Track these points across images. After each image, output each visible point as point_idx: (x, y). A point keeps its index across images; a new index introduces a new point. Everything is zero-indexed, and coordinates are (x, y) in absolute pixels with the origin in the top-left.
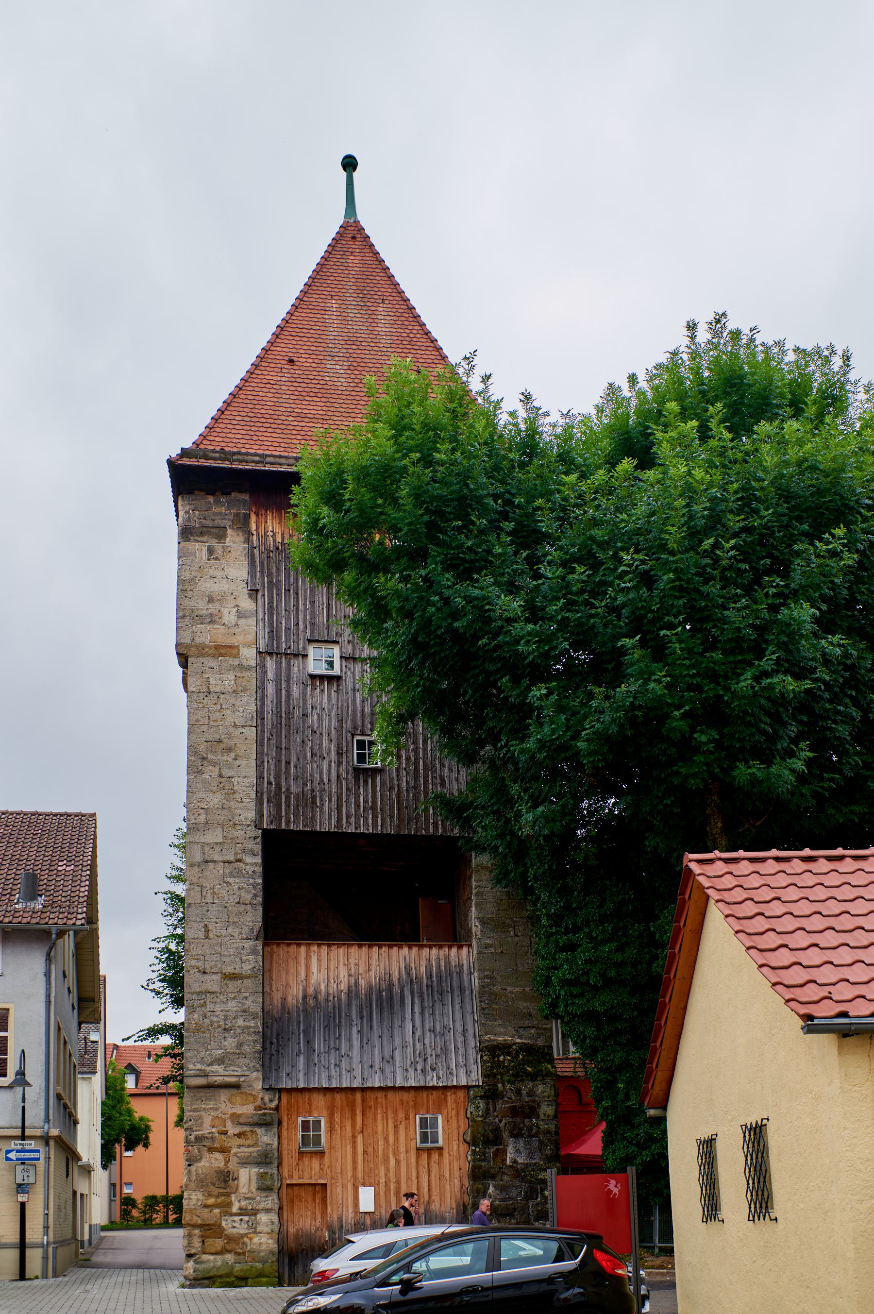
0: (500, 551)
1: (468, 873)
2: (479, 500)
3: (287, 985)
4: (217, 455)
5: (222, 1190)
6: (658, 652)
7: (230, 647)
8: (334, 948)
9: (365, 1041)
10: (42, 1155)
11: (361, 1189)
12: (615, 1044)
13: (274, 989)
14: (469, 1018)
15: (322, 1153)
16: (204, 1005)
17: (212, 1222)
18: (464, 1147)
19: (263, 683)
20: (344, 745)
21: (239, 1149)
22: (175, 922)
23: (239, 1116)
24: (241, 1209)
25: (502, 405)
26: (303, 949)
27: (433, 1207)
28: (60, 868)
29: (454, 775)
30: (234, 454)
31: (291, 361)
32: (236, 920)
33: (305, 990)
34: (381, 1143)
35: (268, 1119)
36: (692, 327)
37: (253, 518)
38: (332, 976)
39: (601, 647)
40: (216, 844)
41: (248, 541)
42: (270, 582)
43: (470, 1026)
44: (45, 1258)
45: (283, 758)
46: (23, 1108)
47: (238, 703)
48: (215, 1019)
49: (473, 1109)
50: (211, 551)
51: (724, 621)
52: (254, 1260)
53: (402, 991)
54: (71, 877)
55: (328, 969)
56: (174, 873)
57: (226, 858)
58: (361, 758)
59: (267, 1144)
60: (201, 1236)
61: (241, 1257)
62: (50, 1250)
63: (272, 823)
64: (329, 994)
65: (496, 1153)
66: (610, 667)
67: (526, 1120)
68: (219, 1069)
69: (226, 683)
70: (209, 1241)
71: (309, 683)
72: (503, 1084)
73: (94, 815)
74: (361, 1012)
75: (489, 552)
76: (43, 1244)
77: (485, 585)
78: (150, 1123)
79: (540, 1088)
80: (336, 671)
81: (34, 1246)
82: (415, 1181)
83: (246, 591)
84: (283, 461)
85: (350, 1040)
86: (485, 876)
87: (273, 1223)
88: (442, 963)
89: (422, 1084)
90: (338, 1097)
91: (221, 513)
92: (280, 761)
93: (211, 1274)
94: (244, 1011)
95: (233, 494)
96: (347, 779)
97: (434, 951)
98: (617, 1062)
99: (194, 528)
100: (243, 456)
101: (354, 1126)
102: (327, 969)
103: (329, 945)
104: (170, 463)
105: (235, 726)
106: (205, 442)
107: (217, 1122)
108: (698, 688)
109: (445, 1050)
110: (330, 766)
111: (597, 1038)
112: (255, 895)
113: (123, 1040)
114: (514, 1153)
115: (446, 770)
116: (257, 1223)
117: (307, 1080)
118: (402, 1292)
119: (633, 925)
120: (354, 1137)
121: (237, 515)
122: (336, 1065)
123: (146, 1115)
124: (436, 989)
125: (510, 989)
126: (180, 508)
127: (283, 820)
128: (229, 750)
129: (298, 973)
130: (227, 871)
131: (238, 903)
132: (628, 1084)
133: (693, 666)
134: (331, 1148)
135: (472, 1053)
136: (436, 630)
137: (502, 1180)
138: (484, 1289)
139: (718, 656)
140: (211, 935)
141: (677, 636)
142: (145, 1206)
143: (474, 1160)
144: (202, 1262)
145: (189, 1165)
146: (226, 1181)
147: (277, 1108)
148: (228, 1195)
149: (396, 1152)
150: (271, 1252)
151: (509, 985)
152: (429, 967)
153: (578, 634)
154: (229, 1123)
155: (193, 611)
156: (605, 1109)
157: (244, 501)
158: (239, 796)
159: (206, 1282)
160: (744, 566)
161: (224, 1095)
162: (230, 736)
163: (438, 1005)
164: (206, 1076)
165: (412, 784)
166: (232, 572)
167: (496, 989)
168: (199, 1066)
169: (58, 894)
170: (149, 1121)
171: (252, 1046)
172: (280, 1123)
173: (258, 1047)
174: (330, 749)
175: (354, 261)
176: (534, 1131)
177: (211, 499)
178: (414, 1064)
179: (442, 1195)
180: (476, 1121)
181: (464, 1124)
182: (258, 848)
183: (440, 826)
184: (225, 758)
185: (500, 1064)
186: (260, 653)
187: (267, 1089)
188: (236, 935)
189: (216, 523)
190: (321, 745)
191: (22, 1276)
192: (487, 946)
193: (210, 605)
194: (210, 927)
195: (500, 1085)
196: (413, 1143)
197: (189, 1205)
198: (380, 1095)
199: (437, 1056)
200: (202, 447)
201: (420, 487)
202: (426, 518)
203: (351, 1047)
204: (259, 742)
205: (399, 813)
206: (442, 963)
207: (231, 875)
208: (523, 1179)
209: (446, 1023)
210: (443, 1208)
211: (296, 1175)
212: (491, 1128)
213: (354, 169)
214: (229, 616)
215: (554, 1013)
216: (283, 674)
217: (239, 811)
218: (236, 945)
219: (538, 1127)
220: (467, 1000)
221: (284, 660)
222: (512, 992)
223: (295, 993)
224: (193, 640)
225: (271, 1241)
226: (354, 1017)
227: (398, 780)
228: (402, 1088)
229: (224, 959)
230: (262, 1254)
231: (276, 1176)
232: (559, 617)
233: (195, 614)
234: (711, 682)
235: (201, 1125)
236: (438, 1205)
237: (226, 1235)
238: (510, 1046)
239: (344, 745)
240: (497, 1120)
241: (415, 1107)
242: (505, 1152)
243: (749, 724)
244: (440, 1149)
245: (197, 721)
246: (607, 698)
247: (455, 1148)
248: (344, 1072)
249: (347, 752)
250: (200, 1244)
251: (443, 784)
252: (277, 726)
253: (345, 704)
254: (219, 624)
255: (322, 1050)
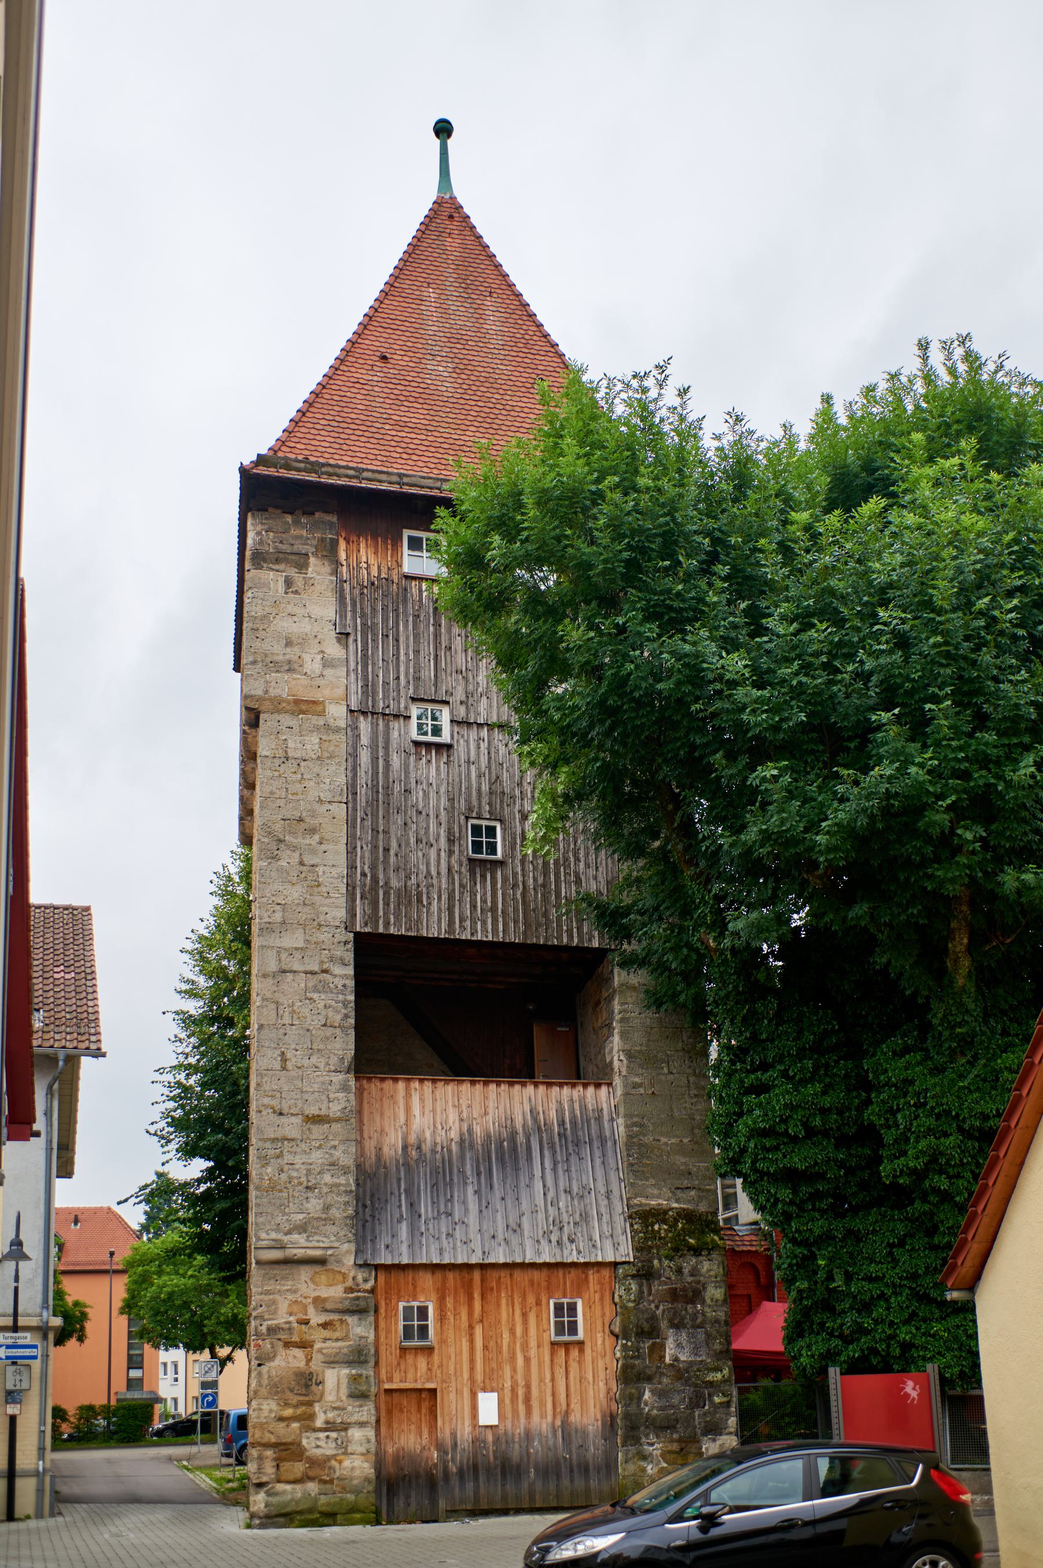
0: (715, 599)
1: (605, 994)
2: (687, 536)
3: (382, 1131)
4: (302, 465)
5: (302, 1398)
6: (918, 727)
7: (314, 702)
8: (440, 1084)
9: (484, 1204)
10: (38, 1352)
11: (481, 1396)
12: (814, 1209)
13: (366, 1136)
14: (613, 1177)
15: (430, 1350)
16: (280, 1156)
17: (289, 1440)
18: (610, 1341)
19: (355, 749)
20: (456, 829)
21: (325, 1345)
22: (188, 1050)
23: (325, 1300)
24: (327, 1422)
25: (705, 424)
26: (401, 1085)
27: (572, 1418)
28: (56, 976)
29: (591, 872)
30: (323, 465)
31: (384, 358)
32: (321, 1047)
33: (405, 1139)
34: (506, 1335)
35: (362, 1304)
36: (924, 346)
37: (342, 545)
38: (438, 1120)
39: (843, 720)
40: (296, 949)
41: (335, 572)
42: (363, 624)
43: (615, 1187)
44: (40, 1491)
45: (381, 843)
46: (16, 1289)
47: (323, 772)
48: (295, 1174)
49: (622, 1292)
50: (288, 583)
51: (997, 695)
52: (344, 1489)
53: (528, 1141)
54: (73, 987)
55: (434, 1111)
56: (185, 987)
57: (308, 968)
58: (477, 847)
59: (361, 1337)
60: (275, 1459)
61: (328, 1486)
62: (48, 1479)
63: (366, 925)
64: (436, 1144)
65: (652, 1349)
66: (852, 745)
67: (689, 1306)
68: (300, 1239)
69: (308, 747)
70: (286, 1466)
71: (413, 750)
72: (660, 1260)
73: (88, 909)
74: (478, 1167)
75: (701, 600)
76: (38, 1471)
77: (701, 641)
78: (87, 1310)
79: (706, 1266)
80: (445, 737)
81: (26, 1474)
82: (550, 1385)
83: (333, 634)
84: (383, 477)
85: (464, 1202)
86: (631, 998)
87: (369, 1441)
88: (577, 1106)
89: (559, 1260)
90: (450, 1275)
91: (301, 537)
92: (375, 847)
93: (288, 1509)
94: (332, 1164)
95: (317, 515)
96: (460, 873)
97: (566, 1090)
98: (817, 1232)
99: (267, 553)
100: (336, 470)
101: (470, 1314)
102: (434, 1112)
103: (434, 1081)
104: (243, 471)
105: (320, 801)
106: (284, 448)
107: (295, 1309)
108: (965, 775)
109: (585, 1217)
110: (439, 855)
111: (792, 1203)
112: (346, 1016)
113: (119, 1203)
114: (675, 1348)
115: (582, 865)
116: (348, 1441)
117: (413, 1255)
118: (703, 1529)
119: (837, 1062)
120: (471, 1327)
121: (322, 540)
122: (448, 1235)
123: (82, 1299)
124: (571, 1139)
125: (664, 1140)
126: (249, 527)
127: (381, 921)
128: (313, 831)
129: (395, 1118)
130: (310, 984)
131: (325, 1025)
132: (831, 1260)
133: (960, 749)
134: (443, 1341)
135: (620, 1222)
136: (632, 692)
137: (660, 1383)
138: (806, 1524)
139: (990, 737)
140: (289, 1065)
141: (942, 712)
142: (79, 1420)
143: (625, 1358)
144: (276, 1494)
145: (259, 1365)
146: (307, 1386)
147: (373, 1291)
148: (310, 1404)
149: (525, 1347)
150: (367, 1479)
151: (663, 1135)
152: (560, 1111)
153: (815, 704)
154: (311, 1310)
155: (266, 656)
156: (800, 1291)
157: (331, 525)
158: (325, 890)
159: (281, 1520)
160: (1021, 632)
161: (305, 1273)
162: (313, 814)
163: (574, 1159)
164: (283, 1248)
165: (540, 881)
166: (316, 610)
167: (648, 1139)
168: (273, 1235)
169: (59, 1009)
170: (86, 1306)
171: (342, 1209)
172: (376, 1311)
173: (351, 1211)
174: (438, 835)
175: (452, 244)
176: (699, 1321)
177: (289, 519)
178: (547, 1234)
179: (583, 1402)
180: (626, 1308)
181: (609, 1310)
182: (350, 957)
183: (575, 935)
184: (307, 841)
185: (655, 1235)
186: (352, 711)
187: (360, 1266)
188: (322, 1066)
189: (295, 549)
190: (427, 828)
191: (10, 1517)
192: (636, 1086)
193: (288, 650)
194: (289, 1055)
195: (656, 1262)
196: (546, 1335)
197: (258, 1417)
198: (503, 1273)
199: (575, 1223)
200: (280, 454)
201: (617, 518)
202: (625, 555)
203: (467, 1211)
204: (351, 823)
205: (525, 917)
206: (577, 1106)
207: (315, 990)
208: (687, 1382)
209: (584, 1182)
210: (585, 1420)
211: (397, 1376)
212: (646, 1316)
213: (449, 136)
214: (312, 664)
215: (736, 1171)
216: (380, 739)
217: (325, 909)
218: (321, 1079)
219: (703, 1314)
220: (610, 1153)
221: (381, 722)
222: (666, 1144)
223: (392, 1143)
224: (266, 692)
225: (366, 1465)
226: (469, 1173)
227: (524, 876)
228: (533, 1265)
229: (306, 1097)
230: (355, 1482)
231: (372, 1379)
232: (794, 683)
233: (268, 660)
234: (981, 769)
235: (275, 1312)
236: (578, 1415)
237: (308, 1458)
238: (666, 1212)
239: (456, 829)
240: (653, 1306)
241: (548, 1288)
242: (663, 1347)
243: (1024, 821)
244: (581, 1344)
245: (272, 793)
246: (856, 783)
247: (599, 1342)
248: (459, 1244)
249: (460, 838)
250: (274, 1470)
251: (578, 882)
252: (372, 803)
253: (457, 780)
254: (299, 673)
255: (430, 1215)
